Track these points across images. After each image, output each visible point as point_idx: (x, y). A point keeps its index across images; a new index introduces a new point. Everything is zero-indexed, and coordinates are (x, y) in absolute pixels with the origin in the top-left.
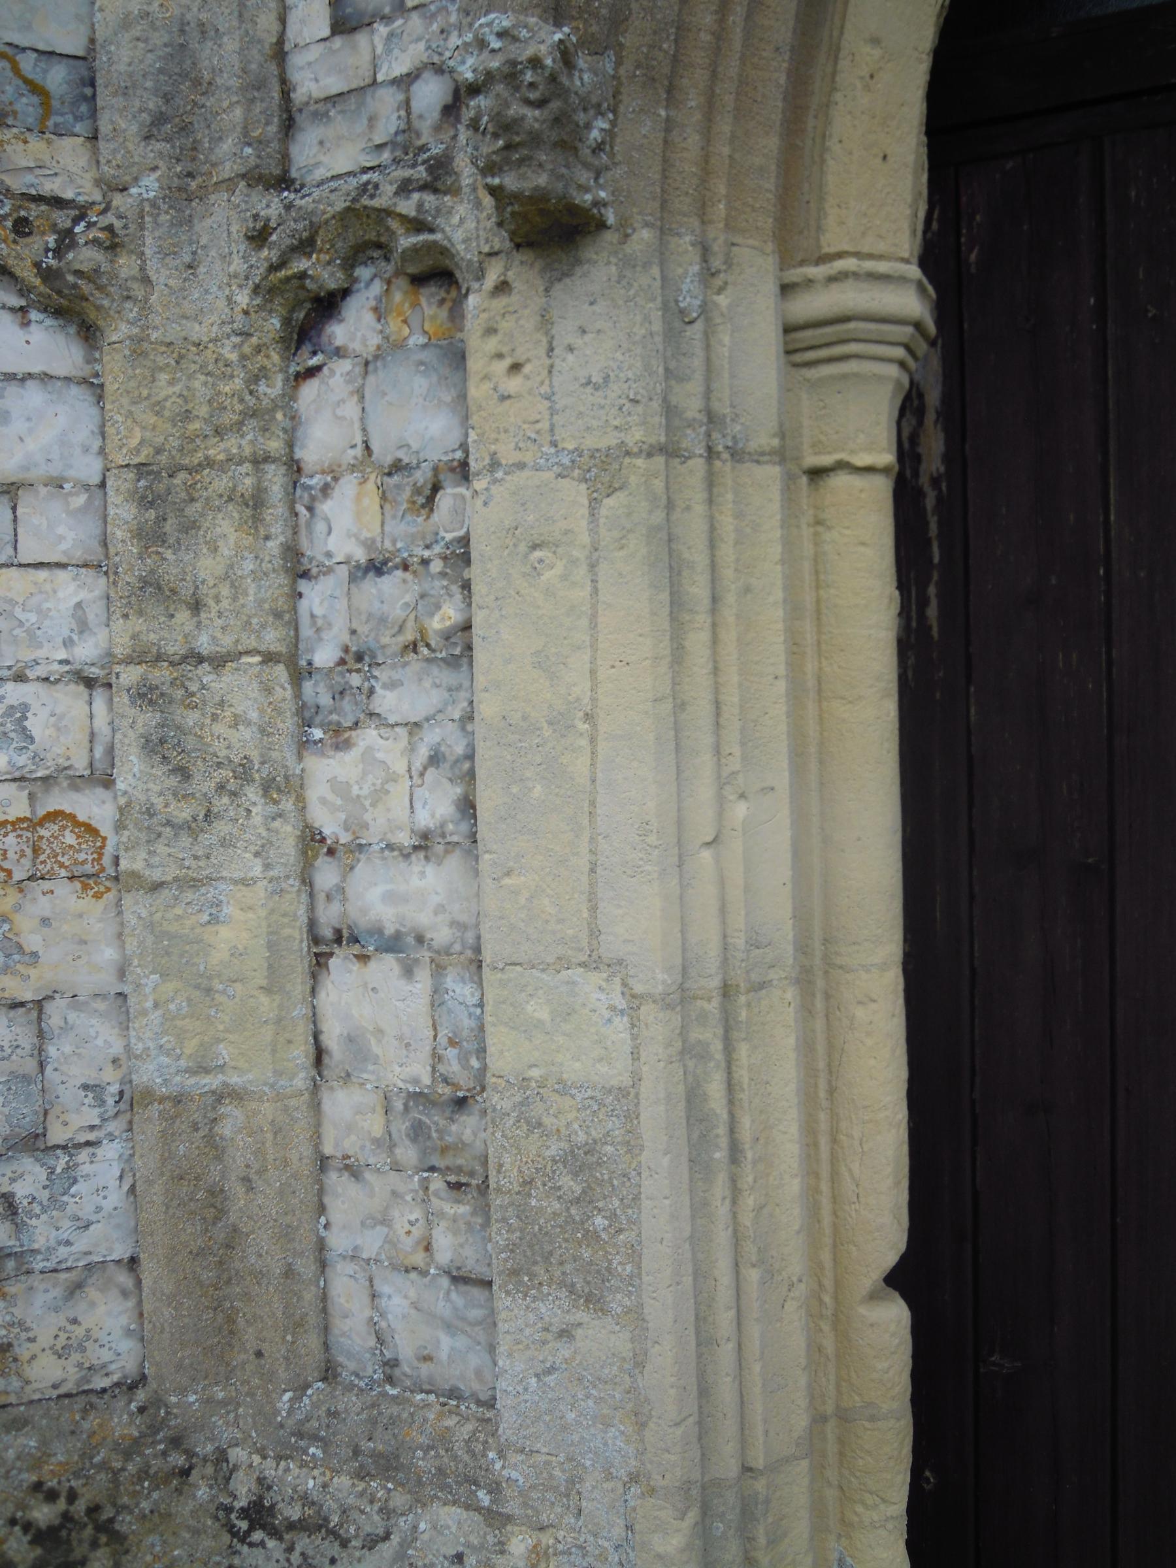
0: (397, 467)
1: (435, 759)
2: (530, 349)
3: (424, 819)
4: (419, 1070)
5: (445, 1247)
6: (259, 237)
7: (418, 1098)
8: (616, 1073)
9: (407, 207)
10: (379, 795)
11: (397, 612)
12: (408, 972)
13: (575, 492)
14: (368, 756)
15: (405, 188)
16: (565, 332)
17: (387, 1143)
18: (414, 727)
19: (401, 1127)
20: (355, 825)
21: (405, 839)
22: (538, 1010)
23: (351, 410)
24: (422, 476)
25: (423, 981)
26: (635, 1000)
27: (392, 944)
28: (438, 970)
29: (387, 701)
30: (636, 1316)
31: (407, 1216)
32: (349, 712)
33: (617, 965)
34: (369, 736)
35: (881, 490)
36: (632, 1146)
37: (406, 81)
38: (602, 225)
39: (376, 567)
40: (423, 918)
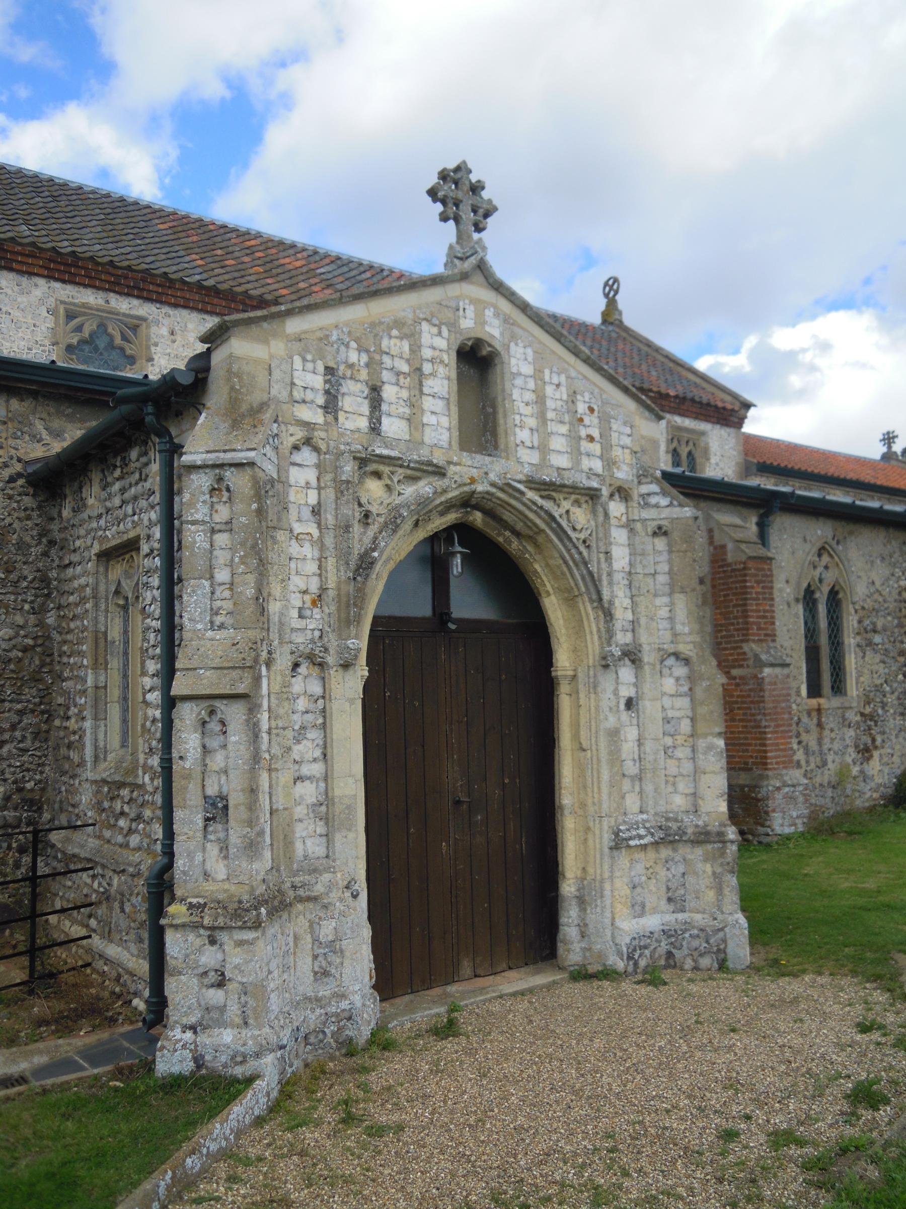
0: (311, 695)
1: (317, 745)
2: (341, 681)
3: (315, 756)
4: (314, 800)
5: (319, 831)
6: (292, 653)
7: (314, 805)
8: (353, 793)
9: (321, 655)
10: (307, 752)
11: (311, 720)
12: (312, 783)
13: (347, 704)
14: (305, 745)
15: (320, 651)
16: (346, 680)
17: (308, 814)
18: (313, 740)
19: (310, 811)
20: (302, 757)
21: (311, 759)
22: (342, 785)
23: (303, 684)
24: (316, 697)
25: (315, 784)
26: (356, 781)
27: (309, 778)
28: (317, 782)
29: (309, 736)
30: (356, 830)
31: (312, 827)
32: (301, 737)
33: (353, 776)
34: (305, 742)
35: (360, 701)
36: (356, 803)
37: (313, 630)
38: (30, 483)
39: (307, 712)
40: (314, 773)
